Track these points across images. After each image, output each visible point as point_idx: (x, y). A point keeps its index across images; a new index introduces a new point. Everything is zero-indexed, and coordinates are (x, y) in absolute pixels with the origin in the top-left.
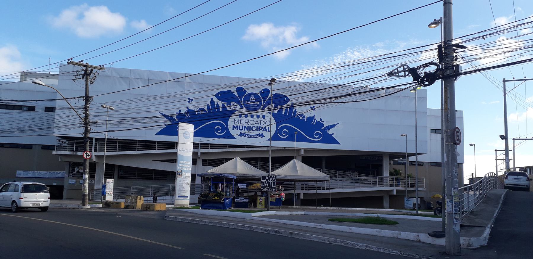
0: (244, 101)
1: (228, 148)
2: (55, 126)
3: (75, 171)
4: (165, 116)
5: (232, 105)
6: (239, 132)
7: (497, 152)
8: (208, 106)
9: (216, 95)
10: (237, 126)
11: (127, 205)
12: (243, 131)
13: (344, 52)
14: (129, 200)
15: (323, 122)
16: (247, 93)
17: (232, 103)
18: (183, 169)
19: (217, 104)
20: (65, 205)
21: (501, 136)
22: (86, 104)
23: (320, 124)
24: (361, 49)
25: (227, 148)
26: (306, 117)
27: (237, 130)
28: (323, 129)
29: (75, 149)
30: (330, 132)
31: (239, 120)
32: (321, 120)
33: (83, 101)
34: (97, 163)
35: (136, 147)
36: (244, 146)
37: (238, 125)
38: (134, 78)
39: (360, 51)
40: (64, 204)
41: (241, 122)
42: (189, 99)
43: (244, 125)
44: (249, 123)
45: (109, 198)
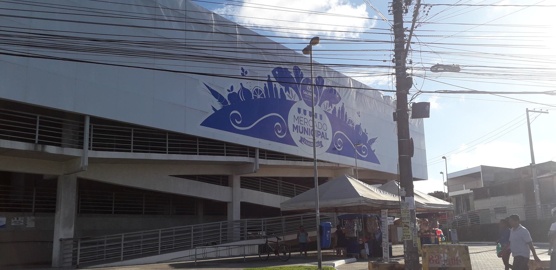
11: (440, 268)
27: (298, 132)
41: (300, 120)
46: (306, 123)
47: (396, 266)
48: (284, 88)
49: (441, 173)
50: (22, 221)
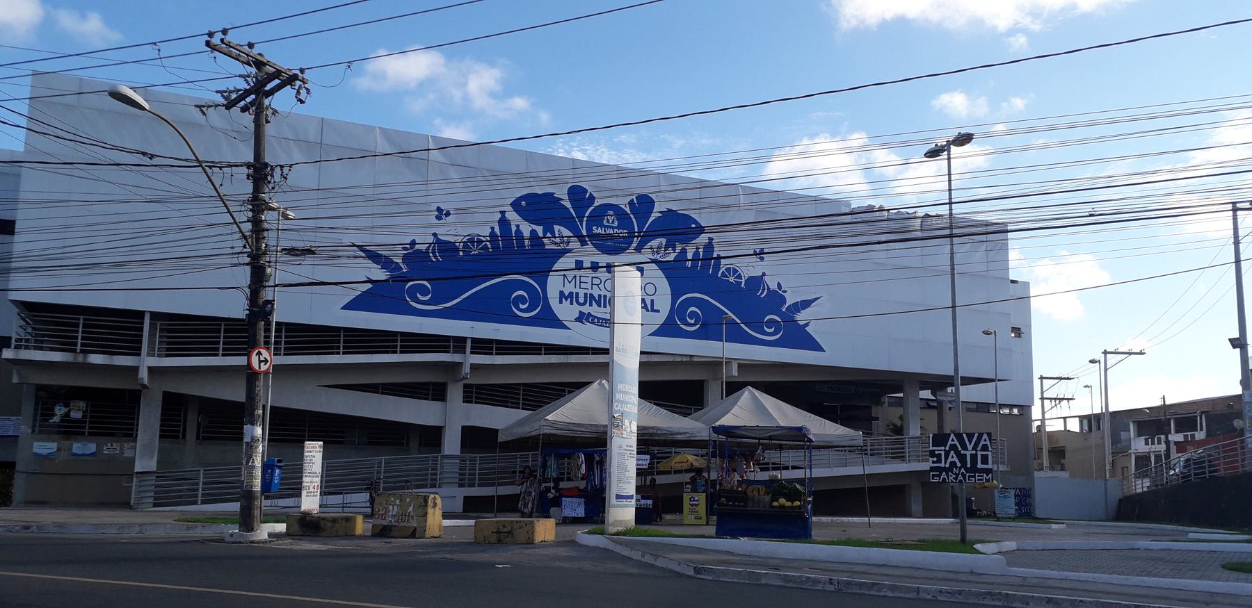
0: (589, 229)
1: (545, 354)
2: (13, 265)
3: (53, 415)
4: (374, 257)
5: (557, 235)
6: (575, 310)
7: (1044, 380)
8: (492, 234)
9: (515, 205)
10: (571, 294)
11: (384, 526)
12: (586, 309)
13: (550, 150)
14: (393, 510)
15: (785, 292)
16: (596, 204)
17: (556, 228)
18: (625, 409)
19: (518, 231)
20: (137, 528)
21: (1231, 340)
22: (257, 189)
23: (776, 298)
24: (587, 146)
25: (541, 354)
26: (743, 278)
27: (572, 303)
28: (784, 310)
29: (82, 345)
30: (801, 317)
31: (575, 276)
32: (779, 285)
33: (248, 178)
34: (144, 391)
35: (218, 343)
36: (587, 349)
37: (575, 291)
38: (276, 135)
39: (587, 150)
40: (133, 525)
41: (580, 282)
42: (439, 209)
43: (589, 292)
44: (601, 286)
45: (310, 502)
46: (597, 285)
47: (308, 518)
48: (539, 230)
49: (1092, 362)
50: (118, 448)
